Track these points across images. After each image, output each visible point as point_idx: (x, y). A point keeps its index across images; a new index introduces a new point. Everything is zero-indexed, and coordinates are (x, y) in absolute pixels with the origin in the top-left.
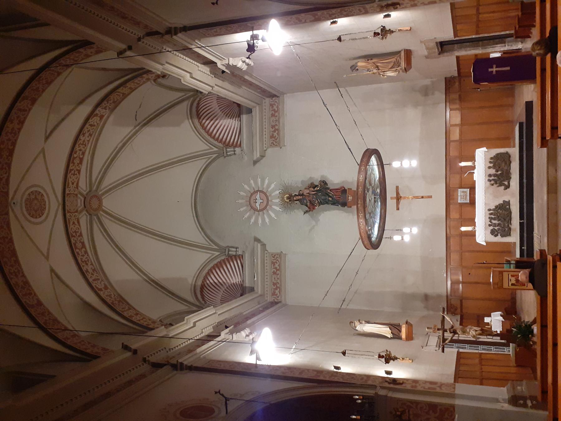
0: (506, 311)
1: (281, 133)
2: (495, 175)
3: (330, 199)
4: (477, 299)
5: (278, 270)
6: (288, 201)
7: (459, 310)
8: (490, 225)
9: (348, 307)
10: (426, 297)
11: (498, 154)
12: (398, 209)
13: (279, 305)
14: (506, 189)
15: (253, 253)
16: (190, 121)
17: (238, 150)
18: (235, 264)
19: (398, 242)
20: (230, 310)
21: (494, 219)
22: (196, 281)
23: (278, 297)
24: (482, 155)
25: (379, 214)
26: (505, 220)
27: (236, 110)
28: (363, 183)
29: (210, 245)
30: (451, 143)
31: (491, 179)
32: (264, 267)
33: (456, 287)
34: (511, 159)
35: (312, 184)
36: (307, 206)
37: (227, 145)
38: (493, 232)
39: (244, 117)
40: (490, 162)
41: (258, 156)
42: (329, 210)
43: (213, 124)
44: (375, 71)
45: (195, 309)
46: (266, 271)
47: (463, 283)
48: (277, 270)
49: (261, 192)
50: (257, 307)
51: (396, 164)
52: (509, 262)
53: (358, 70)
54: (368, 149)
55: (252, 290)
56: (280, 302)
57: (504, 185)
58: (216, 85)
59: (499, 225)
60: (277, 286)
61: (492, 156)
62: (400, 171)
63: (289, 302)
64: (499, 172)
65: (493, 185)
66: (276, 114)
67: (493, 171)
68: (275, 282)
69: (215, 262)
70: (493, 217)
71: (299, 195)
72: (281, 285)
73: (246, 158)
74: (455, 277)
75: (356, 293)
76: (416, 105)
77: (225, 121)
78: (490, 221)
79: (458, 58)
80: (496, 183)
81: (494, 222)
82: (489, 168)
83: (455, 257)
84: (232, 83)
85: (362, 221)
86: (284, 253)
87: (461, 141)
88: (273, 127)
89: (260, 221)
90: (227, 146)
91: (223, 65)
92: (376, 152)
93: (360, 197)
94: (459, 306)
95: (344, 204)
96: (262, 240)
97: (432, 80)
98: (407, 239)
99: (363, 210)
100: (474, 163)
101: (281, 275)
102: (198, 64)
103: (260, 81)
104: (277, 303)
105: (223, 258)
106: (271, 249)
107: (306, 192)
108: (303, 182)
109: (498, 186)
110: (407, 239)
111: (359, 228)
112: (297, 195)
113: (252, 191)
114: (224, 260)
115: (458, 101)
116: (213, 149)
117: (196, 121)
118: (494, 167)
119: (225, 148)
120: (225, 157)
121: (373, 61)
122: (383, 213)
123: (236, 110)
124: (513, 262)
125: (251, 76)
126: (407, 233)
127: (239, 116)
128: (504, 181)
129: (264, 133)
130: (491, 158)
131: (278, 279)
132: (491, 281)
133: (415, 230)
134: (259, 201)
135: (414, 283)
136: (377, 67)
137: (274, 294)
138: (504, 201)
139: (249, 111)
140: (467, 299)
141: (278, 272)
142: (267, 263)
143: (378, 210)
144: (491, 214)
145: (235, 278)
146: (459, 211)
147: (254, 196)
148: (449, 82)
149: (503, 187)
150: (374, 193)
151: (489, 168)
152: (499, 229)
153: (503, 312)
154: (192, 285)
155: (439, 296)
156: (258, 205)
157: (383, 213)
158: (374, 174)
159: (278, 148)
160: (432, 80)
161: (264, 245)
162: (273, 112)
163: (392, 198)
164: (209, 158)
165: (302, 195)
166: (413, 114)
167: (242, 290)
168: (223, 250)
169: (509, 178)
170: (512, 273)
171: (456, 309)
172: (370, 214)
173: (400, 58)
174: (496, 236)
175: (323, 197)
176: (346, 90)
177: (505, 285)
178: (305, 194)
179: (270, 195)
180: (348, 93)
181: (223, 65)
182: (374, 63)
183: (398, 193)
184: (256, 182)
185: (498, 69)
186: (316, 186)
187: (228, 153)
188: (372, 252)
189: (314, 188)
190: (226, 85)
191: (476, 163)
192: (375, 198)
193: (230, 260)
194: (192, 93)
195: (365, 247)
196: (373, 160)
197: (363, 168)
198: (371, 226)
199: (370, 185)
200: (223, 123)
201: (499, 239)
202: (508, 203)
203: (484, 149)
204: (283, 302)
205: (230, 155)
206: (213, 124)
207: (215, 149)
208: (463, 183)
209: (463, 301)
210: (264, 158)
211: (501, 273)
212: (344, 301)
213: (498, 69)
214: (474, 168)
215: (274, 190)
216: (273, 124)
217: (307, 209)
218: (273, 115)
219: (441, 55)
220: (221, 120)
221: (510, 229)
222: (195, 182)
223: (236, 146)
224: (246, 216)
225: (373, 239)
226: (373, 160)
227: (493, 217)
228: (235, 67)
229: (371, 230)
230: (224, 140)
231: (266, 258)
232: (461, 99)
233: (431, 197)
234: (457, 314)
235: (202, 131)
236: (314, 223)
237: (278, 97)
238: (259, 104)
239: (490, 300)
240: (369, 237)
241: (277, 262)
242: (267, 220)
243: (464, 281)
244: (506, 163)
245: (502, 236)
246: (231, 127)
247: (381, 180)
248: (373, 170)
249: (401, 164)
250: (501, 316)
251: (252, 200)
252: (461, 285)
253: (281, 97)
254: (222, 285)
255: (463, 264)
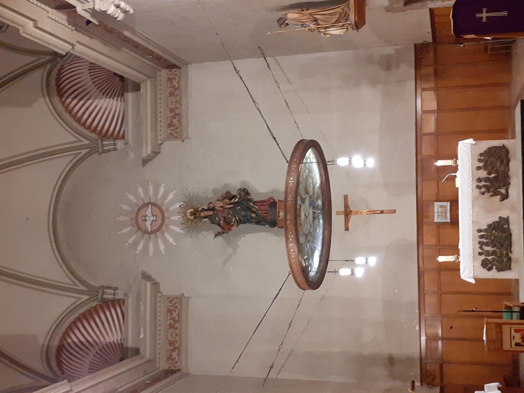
0: (505, 381)
1: (184, 120)
2: (486, 180)
3: (253, 215)
4: (463, 363)
5: (178, 321)
6: (192, 218)
7: (438, 380)
8: (480, 254)
9: (279, 377)
10: (391, 361)
11: (490, 149)
12: (347, 229)
13: (177, 375)
14: (503, 200)
15: (139, 297)
16: (47, 99)
17: (120, 143)
18: (113, 314)
19: (346, 277)
20: (96, 384)
21: (487, 244)
22: (49, 341)
23: (176, 363)
24: (467, 150)
25: (321, 237)
26: (502, 246)
27: (118, 85)
28: (294, 188)
29: (75, 285)
30: (423, 137)
31: (481, 184)
32: (155, 318)
33: (433, 344)
34: (510, 155)
35: (228, 193)
36: (219, 225)
37: (104, 135)
38: (485, 264)
39: (130, 96)
40: (480, 161)
41: (149, 152)
42: (252, 232)
43: (84, 105)
44: (313, 26)
45: (46, 383)
46: (158, 323)
47: (443, 339)
48: (176, 322)
49: (154, 204)
50: (141, 379)
51: (342, 162)
52: (510, 309)
53: (287, 24)
54: (301, 141)
55: (137, 352)
56: (179, 370)
57: (500, 193)
58: (78, 42)
59: (494, 253)
60: (175, 346)
61: (482, 151)
62: (349, 171)
63: (193, 369)
64: (493, 175)
65: (483, 194)
66: (176, 91)
67: (483, 174)
68: (172, 339)
69: (82, 311)
70: (485, 241)
71: (209, 209)
72: (180, 345)
73: (132, 155)
74: (432, 331)
75: (290, 355)
76: (374, 82)
77: (102, 101)
78: (480, 248)
79: (431, 11)
80: (489, 191)
81: (486, 248)
82: (479, 168)
83: (431, 301)
84: (105, 42)
85: (293, 246)
86: (186, 295)
87: (437, 134)
88: (172, 110)
89: (151, 249)
90: (104, 137)
91: (85, 10)
92: (314, 145)
93: (290, 213)
94: (438, 374)
95: (273, 224)
96: (153, 277)
97: (398, 47)
98: (359, 273)
99: (293, 229)
100: (456, 162)
101: (181, 329)
102: (47, 8)
103: (147, 40)
104: (174, 372)
105: (94, 304)
106: (167, 290)
107: (218, 205)
108: (214, 191)
109: (491, 196)
110: (359, 273)
111: (289, 256)
112: (206, 210)
113: (140, 204)
114: (95, 308)
115: (433, 78)
116: (82, 141)
117: (56, 99)
118: (485, 167)
119: (99, 142)
120: (100, 154)
121: (309, 11)
122: (326, 236)
123: (118, 85)
124: (516, 309)
125: (134, 32)
126: (360, 266)
127: (122, 95)
128: (500, 187)
129: (159, 119)
130: (481, 155)
131: (176, 335)
132: (484, 338)
133: (373, 261)
134: (150, 219)
135: (373, 340)
136: (316, 20)
137: (170, 358)
138: (500, 218)
139: (137, 87)
140: (449, 362)
141: (177, 325)
142: (160, 311)
143: (320, 231)
144: (482, 237)
145: (113, 334)
146: (436, 234)
147: (142, 212)
148: (420, 50)
149: (498, 197)
150: (313, 205)
151: (479, 168)
152: (494, 259)
153: (501, 383)
154: (43, 345)
155: (409, 360)
156: (148, 224)
157: (326, 236)
158: (313, 178)
159: (179, 142)
160: (398, 47)
161: (156, 285)
162: (172, 89)
163: (338, 213)
164: (77, 155)
165: (213, 209)
166: (369, 96)
167: (122, 353)
168: (93, 292)
169: (507, 184)
170: (514, 327)
171: (434, 379)
172: (306, 236)
173: (349, 8)
174: (490, 269)
175: (243, 213)
176: (277, 61)
177: (506, 346)
178: (217, 208)
179: (167, 210)
180: (279, 65)
181: (85, 10)
182: (311, 14)
183: (346, 206)
184: (146, 191)
185: (489, 15)
186: (234, 197)
187: (105, 148)
188: (310, 292)
189: (231, 199)
190: (96, 44)
191: (459, 162)
192: (314, 213)
193: (105, 308)
194: (48, 58)
195: (299, 286)
196: (310, 155)
197: (294, 166)
198: (308, 254)
199: (307, 192)
200: (103, 104)
201: (494, 274)
202: (506, 221)
203: (471, 141)
204: (184, 370)
205: (109, 151)
206: (84, 105)
207: (86, 142)
208: (440, 194)
209: (444, 365)
210: (158, 157)
211: (499, 326)
212: (271, 367)
213: (489, 15)
214: (455, 169)
215: (173, 202)
216: (172, 107)
217: (219, 229)
218: (171, 94)
219: (408, 7)
220: (95, 99)
221: (510, 259)
222: (54, 190)
223: (117, 138)
224: (130, 241)
225: (312, 274)
226: (310, 155)
227: (485, 241)
228: (104, 13)
229: (308, 260)
230: (99, 128)
231: (158, 304)
232: (437, 75)
233: (394, 212)
234: (436, 386)
235: (67, 116)
236: (230, 251)
237: (179, 68)
238: (149, 77)
239: (481, 364)
240: (305, 271)
241: (175, 309)
242: (162, 247)
243: (444, 336)
244: (502, 162)
245: (499, 270)
246: (111, 110)
247: (324, 187)
248: (310, 171)
249: (350, 161)
250: (499, 389)
251: (140, 216)
252: (440, 343)
253: (183, 69)
254: (92, 345)
255: (443, 312)
